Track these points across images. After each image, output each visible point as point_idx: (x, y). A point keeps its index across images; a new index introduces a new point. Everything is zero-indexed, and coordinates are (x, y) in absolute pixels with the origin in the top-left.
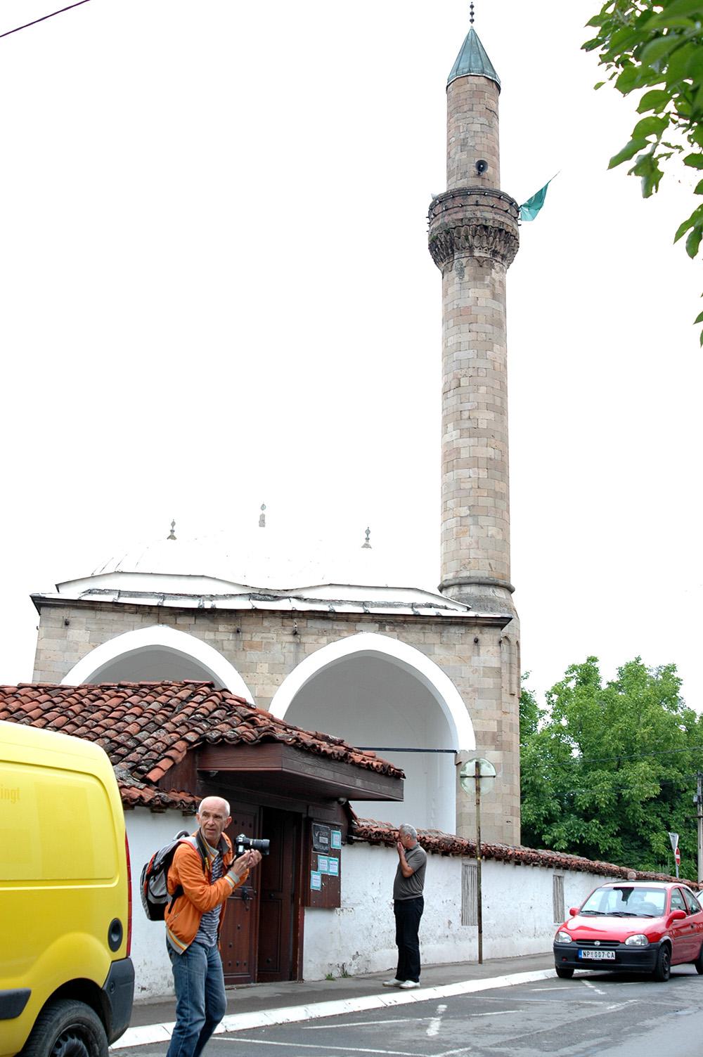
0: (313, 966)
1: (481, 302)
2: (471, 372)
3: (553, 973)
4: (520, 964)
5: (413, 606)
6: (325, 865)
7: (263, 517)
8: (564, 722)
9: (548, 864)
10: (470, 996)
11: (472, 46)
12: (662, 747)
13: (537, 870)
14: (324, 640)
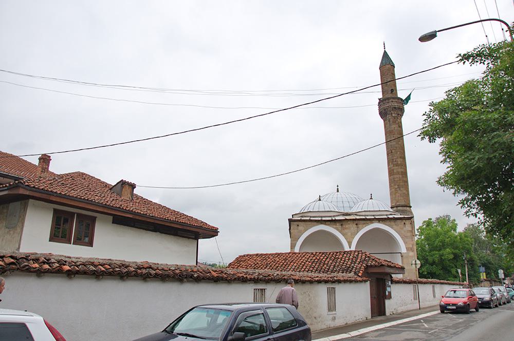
0: (388, 312)
1: (396, 129)
2: (395, 148)
3: (439, 311)
4: (432, 309)
5: (387, 215)
6: (388, 289)
7: (338, 189)
8: (423, 237)
9: (431, 283)
10: (382, 320)
11: (385, 55)
12: (453, 245)
13: (429, 285)
14: (364, 226)
